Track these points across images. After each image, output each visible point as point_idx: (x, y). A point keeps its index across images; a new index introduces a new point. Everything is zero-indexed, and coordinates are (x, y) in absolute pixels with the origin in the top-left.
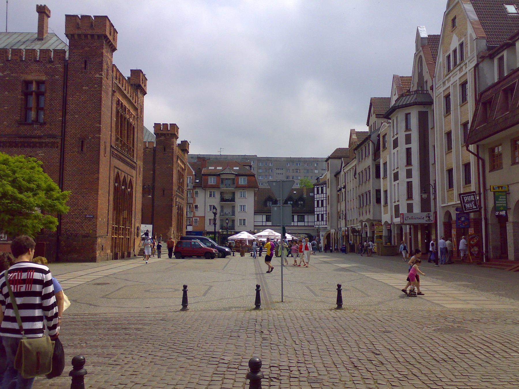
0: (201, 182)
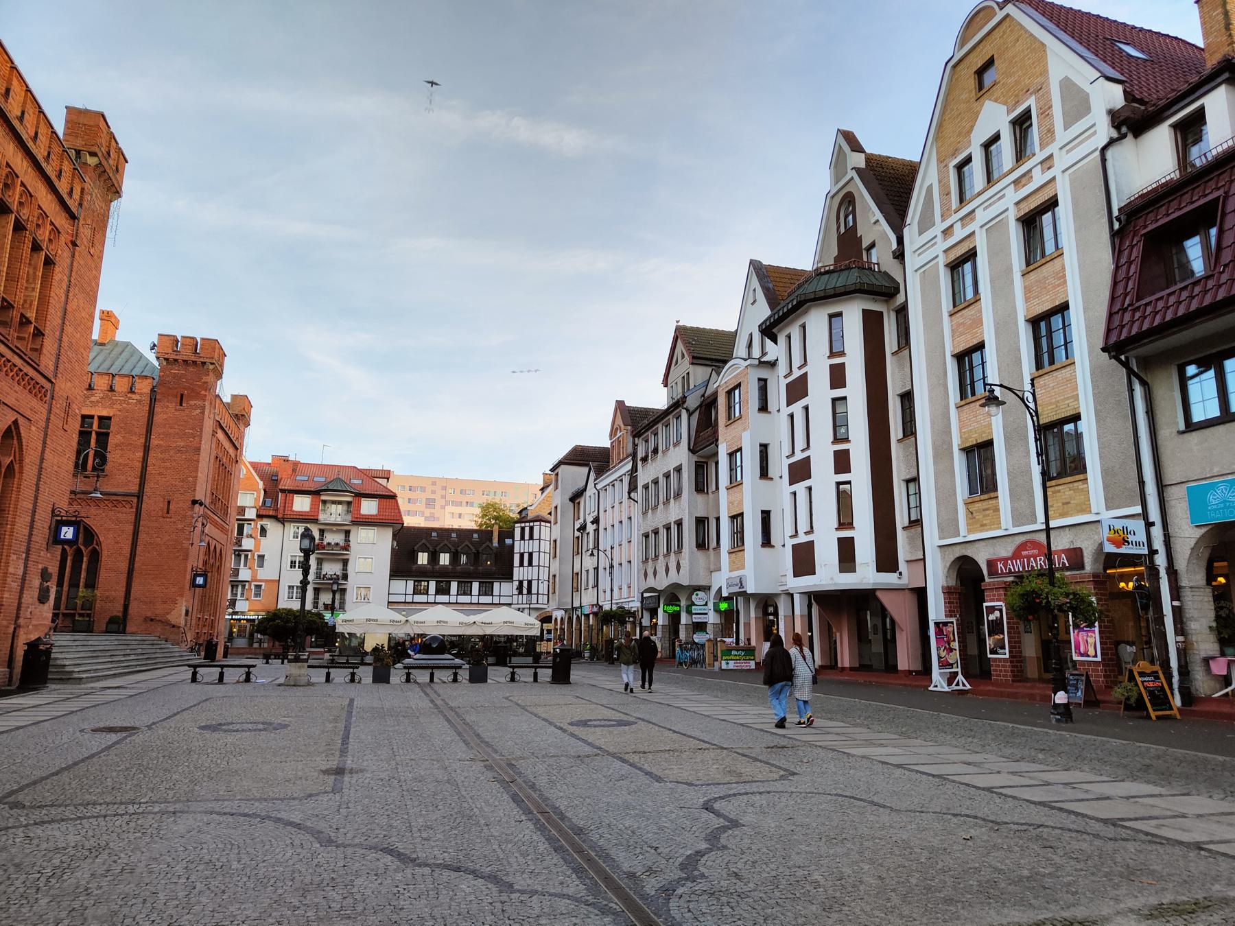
0: (275, 509)
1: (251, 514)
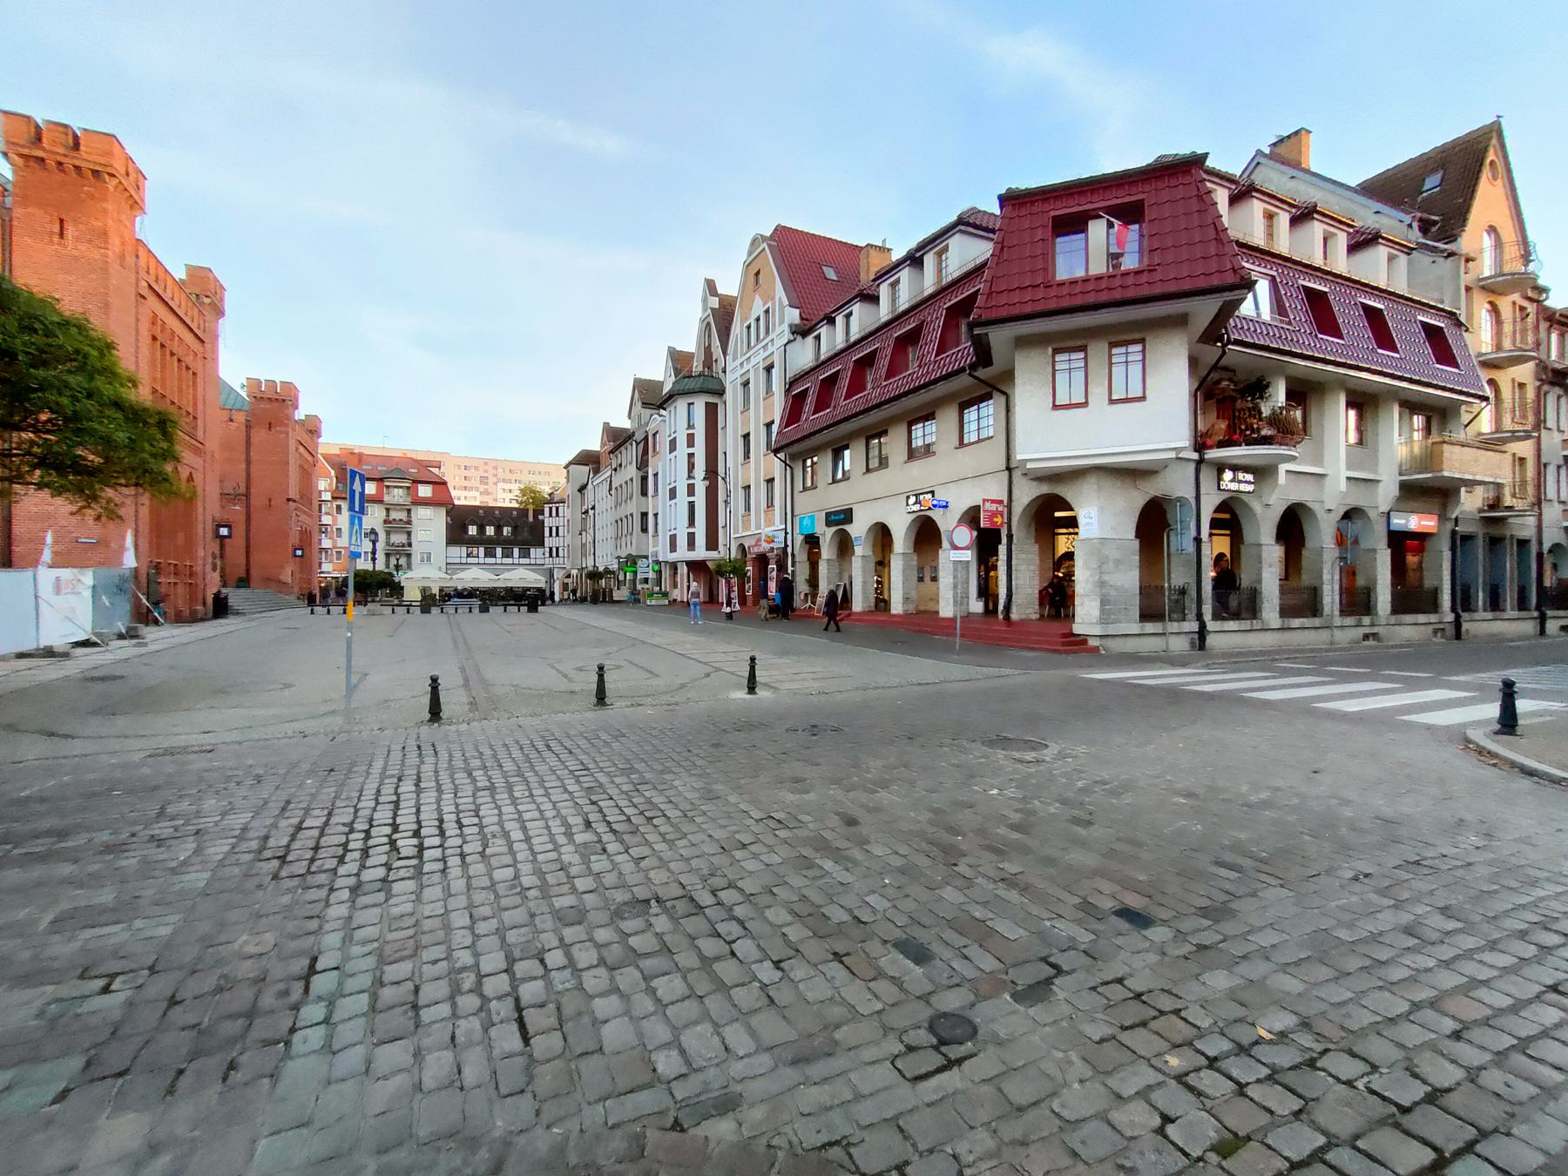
1: (327, 496)
